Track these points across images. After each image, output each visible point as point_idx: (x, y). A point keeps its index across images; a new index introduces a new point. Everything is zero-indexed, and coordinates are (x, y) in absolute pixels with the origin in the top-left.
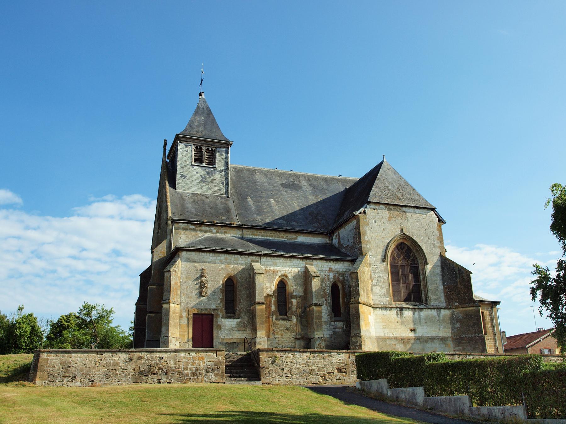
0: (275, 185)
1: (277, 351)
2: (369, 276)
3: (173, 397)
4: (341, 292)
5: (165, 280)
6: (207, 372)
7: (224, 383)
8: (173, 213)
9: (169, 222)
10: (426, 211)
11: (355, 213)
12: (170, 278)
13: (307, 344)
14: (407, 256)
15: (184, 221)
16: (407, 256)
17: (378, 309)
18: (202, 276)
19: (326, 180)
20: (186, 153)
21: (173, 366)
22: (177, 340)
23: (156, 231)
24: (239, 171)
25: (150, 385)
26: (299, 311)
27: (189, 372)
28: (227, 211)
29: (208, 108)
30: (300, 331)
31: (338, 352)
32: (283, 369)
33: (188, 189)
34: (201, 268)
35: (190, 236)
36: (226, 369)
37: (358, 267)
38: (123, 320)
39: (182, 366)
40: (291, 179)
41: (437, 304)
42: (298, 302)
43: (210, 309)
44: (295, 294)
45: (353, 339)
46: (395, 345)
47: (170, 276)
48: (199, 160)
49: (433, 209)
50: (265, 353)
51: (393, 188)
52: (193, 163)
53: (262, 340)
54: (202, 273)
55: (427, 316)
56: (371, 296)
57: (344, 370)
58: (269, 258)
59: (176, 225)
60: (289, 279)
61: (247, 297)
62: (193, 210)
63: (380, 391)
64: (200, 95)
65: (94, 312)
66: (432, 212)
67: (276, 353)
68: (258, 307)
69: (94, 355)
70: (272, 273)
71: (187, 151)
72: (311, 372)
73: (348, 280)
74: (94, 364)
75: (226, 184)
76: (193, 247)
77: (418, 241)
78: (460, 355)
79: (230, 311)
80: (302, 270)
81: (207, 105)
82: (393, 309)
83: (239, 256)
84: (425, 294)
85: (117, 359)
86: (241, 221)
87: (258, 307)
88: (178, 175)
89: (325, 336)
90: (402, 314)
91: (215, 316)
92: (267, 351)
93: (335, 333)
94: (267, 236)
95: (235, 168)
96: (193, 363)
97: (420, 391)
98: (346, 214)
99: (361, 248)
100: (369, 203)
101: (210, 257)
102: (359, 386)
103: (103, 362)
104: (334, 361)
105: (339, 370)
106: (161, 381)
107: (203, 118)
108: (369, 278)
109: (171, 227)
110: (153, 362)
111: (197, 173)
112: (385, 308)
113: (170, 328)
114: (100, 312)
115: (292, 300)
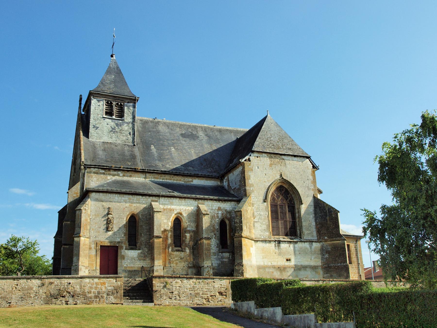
0: (176, 135)
1: (168, 277)
2: (252, 214)
3: (73, 315)
4: (228, 228)
5: (77, 217)
6: (108, 295)
7: (122, 304)
8: (86, 159)
9: (82, 167)
10: (302, 159)
11: (240, 160)
12: (81, 215)
13: (197, 271)
14: (285, 196)
15: (95, 167)
16: (285, 196)
17: (259, 242)
18: (108, 214)
19: (220, 131)
20: (98, 107)
21: (79, 290)
22: (86, 268)
23: (72, 174)
24: (144, 123)
25: (59, 306)
26: (192, 243)
27: (92, 295)
28: (133, 157)
29: (118, 68)
30: (192, 260)
31: (220, 279)
32: (173, 293)
33: (100, 138)
34: (108, 207)
35: (100, 179)
36: (124, 293)
37: (242, 207)
38: (46, 251)
39: (86, 291)
40: (190, 130)
41: (310, 238)
42: (191, 236)
43: (115, 242)
44: (188, 229)
45: (236, 268)
46: (273, 272)
47: (81, 213)
48: (109, 113)
49: (308, 158)
50: (157, 279)
51: (275, 139)
52: (105, 116)
53: (159, 268)
54: (109, 211)
55: (301, 248)
56: (253, 231)
57: (224, 294)
58: (166, 198)
59: (88, 170)
60: (183, 216)
61: (147, 232)
62: (103, 157)
63: (249, 311)
64: (112, 56)
65: (20, 244)
66: (308, 160)
67: (167, 279)
68: (156, 240)
69: (12, 281)
70: (168, 211)
71: (99, 106)
72: (197, 295)
73: (234, 218)
74: (11, 289)
75: (133, 134)
76: (101, 189)
77: (295, 185)
78: (324, 281)
79: (133, 243)
80: (195, 209)
81: (117, 65)
82: (272, 242)
83: (141, 197)
84: (300, 230)
85: (31, 285)
86: (145, 166)
87: (156, 240)
88: (91, 126)
89: (214, 265)
90: (280, 246)
91: (119, 248)
92: (160, 277)
93: (222, 262)
94: (167, 179)
95: (141, 120)
96: (96, 288)
97: (279, 310)
98: (235, 160)
99: (245, 191)
100: (253, 152)
101: (116, 197)
102: (233, 307)
103: (19, 287)
104: (216, 286)
105: (221, 293)
106: (69, 303)
107: (113, 76)
108: (252, 216)
109: (84, 171)
110: (62, 287)
111: (107, 124)
112: (265, 241)
113: (80, 258)
114: (25, 243)
115: (186, 234)
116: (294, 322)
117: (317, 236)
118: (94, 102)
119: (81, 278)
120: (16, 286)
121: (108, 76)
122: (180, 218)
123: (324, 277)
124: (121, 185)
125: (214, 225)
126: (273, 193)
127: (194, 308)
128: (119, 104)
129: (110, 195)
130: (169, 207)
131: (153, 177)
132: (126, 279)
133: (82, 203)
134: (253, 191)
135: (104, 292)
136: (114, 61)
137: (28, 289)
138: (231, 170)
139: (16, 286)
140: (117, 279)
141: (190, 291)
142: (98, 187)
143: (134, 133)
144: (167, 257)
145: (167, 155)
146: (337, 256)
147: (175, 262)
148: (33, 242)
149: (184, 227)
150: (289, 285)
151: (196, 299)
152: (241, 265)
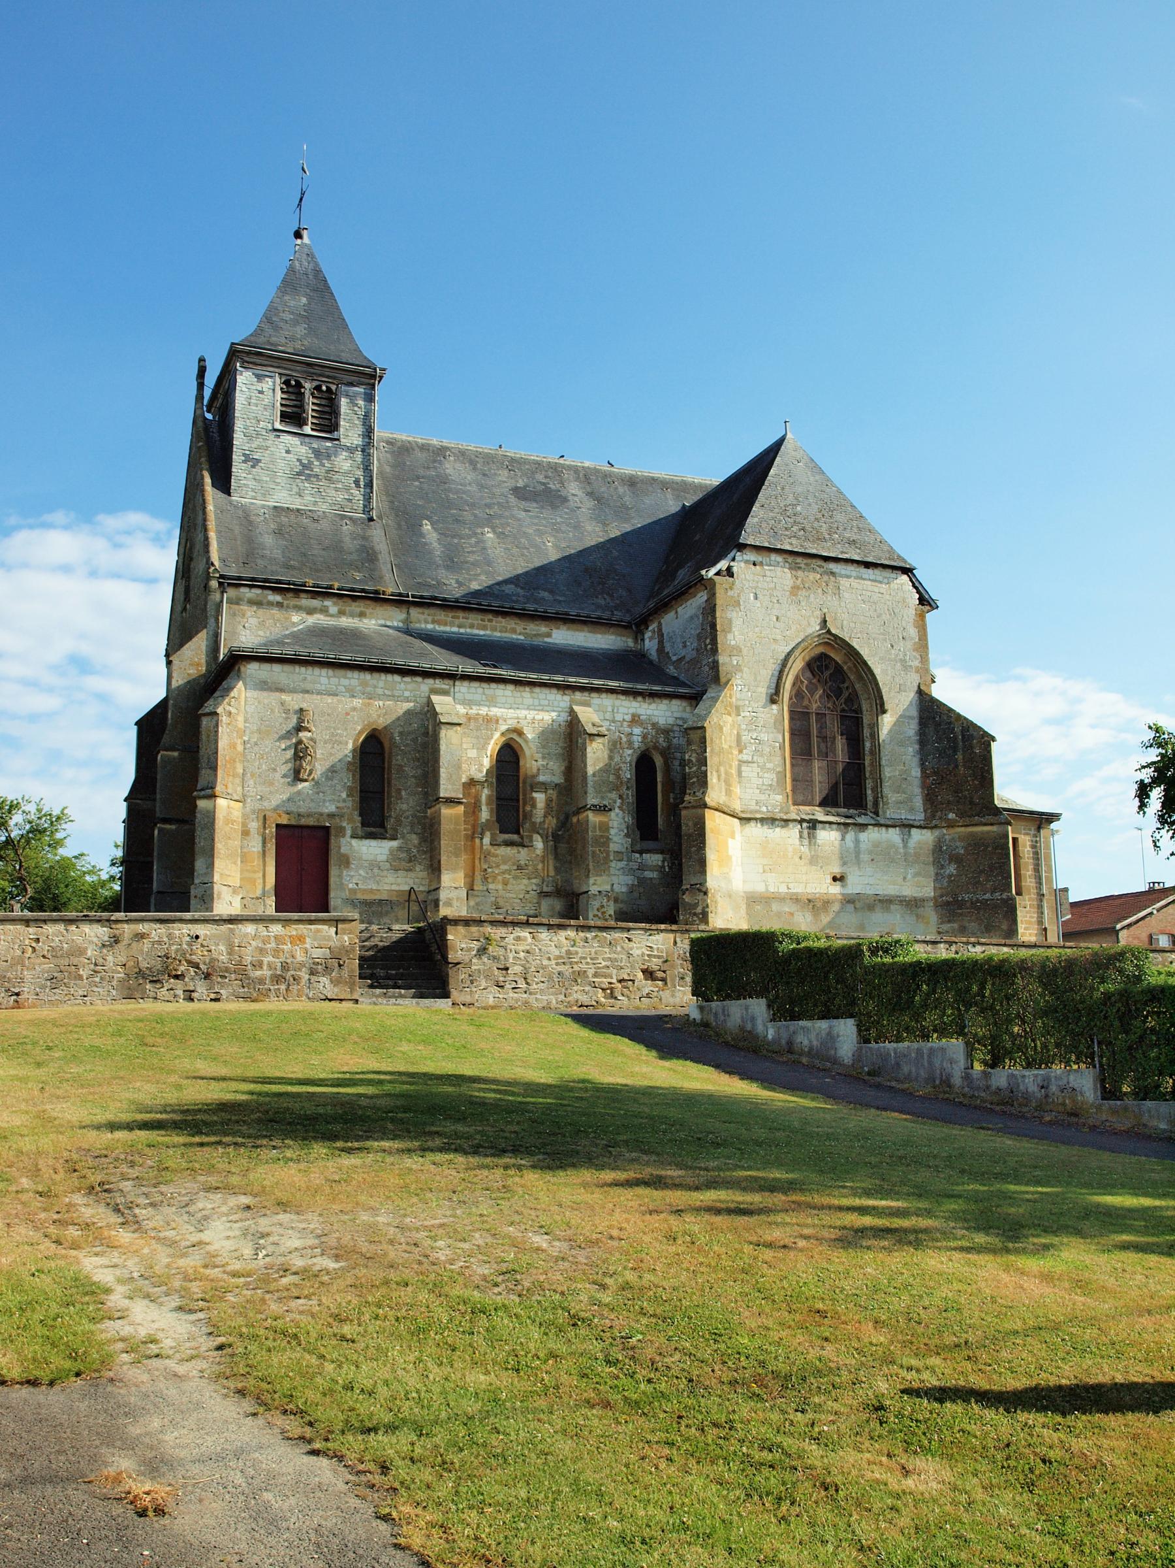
0: (497, 491)
2: (734, 738)
3: (225, 1034)
4: (659, 779)
5: (204, 737)
7: (357, 1001)
8: (223, 560)
9: (214, 584)
10: (888, 573)
11: (703, 572)
12: (217, 732)
13: (569, 906)
14: (834, 685)
15: (254, 583)
16: (834, 685)
17: (753, 824)
18: (299, 728)
19: (632, 482)
20: (257, 397)
21: (224, 958)
23: (179, 608)
24: (401, 451)
25: (165, 1004)
26: (551, 822)
27: (266, 972)
28: (369, 556)
29: (318, 272)
30: (552, 873)
31: (646, 930)
32: (507, 969)
33: (264, 495)
34: (297, 707)
35: (269, 622)
36: (361, 967)
38: (95, 836)
39: (248, 959)
40: (540, 477)
41: (904, 815)
42: (549, 801)
43: (321, 814)
44: (541, 778)
46: (792, 914)
47: (217, 725)
48: (293, 416)
49: (907, 571)
51: (808, 510)
52: (278, 426)
53: (453, 894)
54: (301, 720)
55: (877, 845)
56: (737, 790)
57: (660, 974)
58: (476, 684)
59: (231, 592)
60: (526, 741)
62: (277, 554)
63: (749, 1027)
64: (298, 235)
65: (17, 818)
66: (905, 577)
67: (488, 929)
68: (446, 812)
69: (20, 927)
70: (483, 724)
71: (261, 392)
73: (679, 748)
74: (19, 953)
76: (276, 651)
77: (865, 653)
78: (951, 943)
80: (561, 719)
81: (317, 264)
82: (791, 825)
83: (397, 678)
85: (79, 940)
86: (404, 586)
87: (446, 812)
88: (237, 457)
90: (815, 837)
91: (333, 832)
92: (467, 922)
93: (642, 881)
94: (472, 626)
96: (276, 952)
97: (846, 1030)
98: (681, 573)
99: (715, 666)
100: (742, 547)
101: (323, 678)
102: (695, 1015)
103: (43, 947)
104: (636, 952)
105: (649, 974)
106: (194, 995)
107: (304, 300)
108: (734, 744)
109: (217, 596)
110: (174, 948)
111: (288, 452)
112: (770, 821)
114: (33, 817)
115: (535, 795)
116: (898, 1064)
117: (925, 811)
118: (244, 379)
119: (232, 920)
120: (34, 944)
121: (287, 298)
122: (515, 746)
123: (939, 933)
124: (334, 639)
125: (620, 769)
126: (797, 677)
127: (566, 1016)
128: (324, 388)
129: (303, 669)
130: (484, 711)
131: (430, 619)
132: (363, 926)
133: (217, 694)
134: (738, 668)
135: (302, 965)
136: (306, 250)
137: (70, 954)
138: (670, 601)
139: (34, 944)
140: (340, 926)
141: (557, 964)
142: (265, 645)
143: (371, 481)
144: (477, 862)
145: (473, 552)
146: (981, 872)
147: (500, 878)
148: (54, 813)
149: (529, 773)
150: (880, 953)
151: (575, 988)
152: (700, 890)
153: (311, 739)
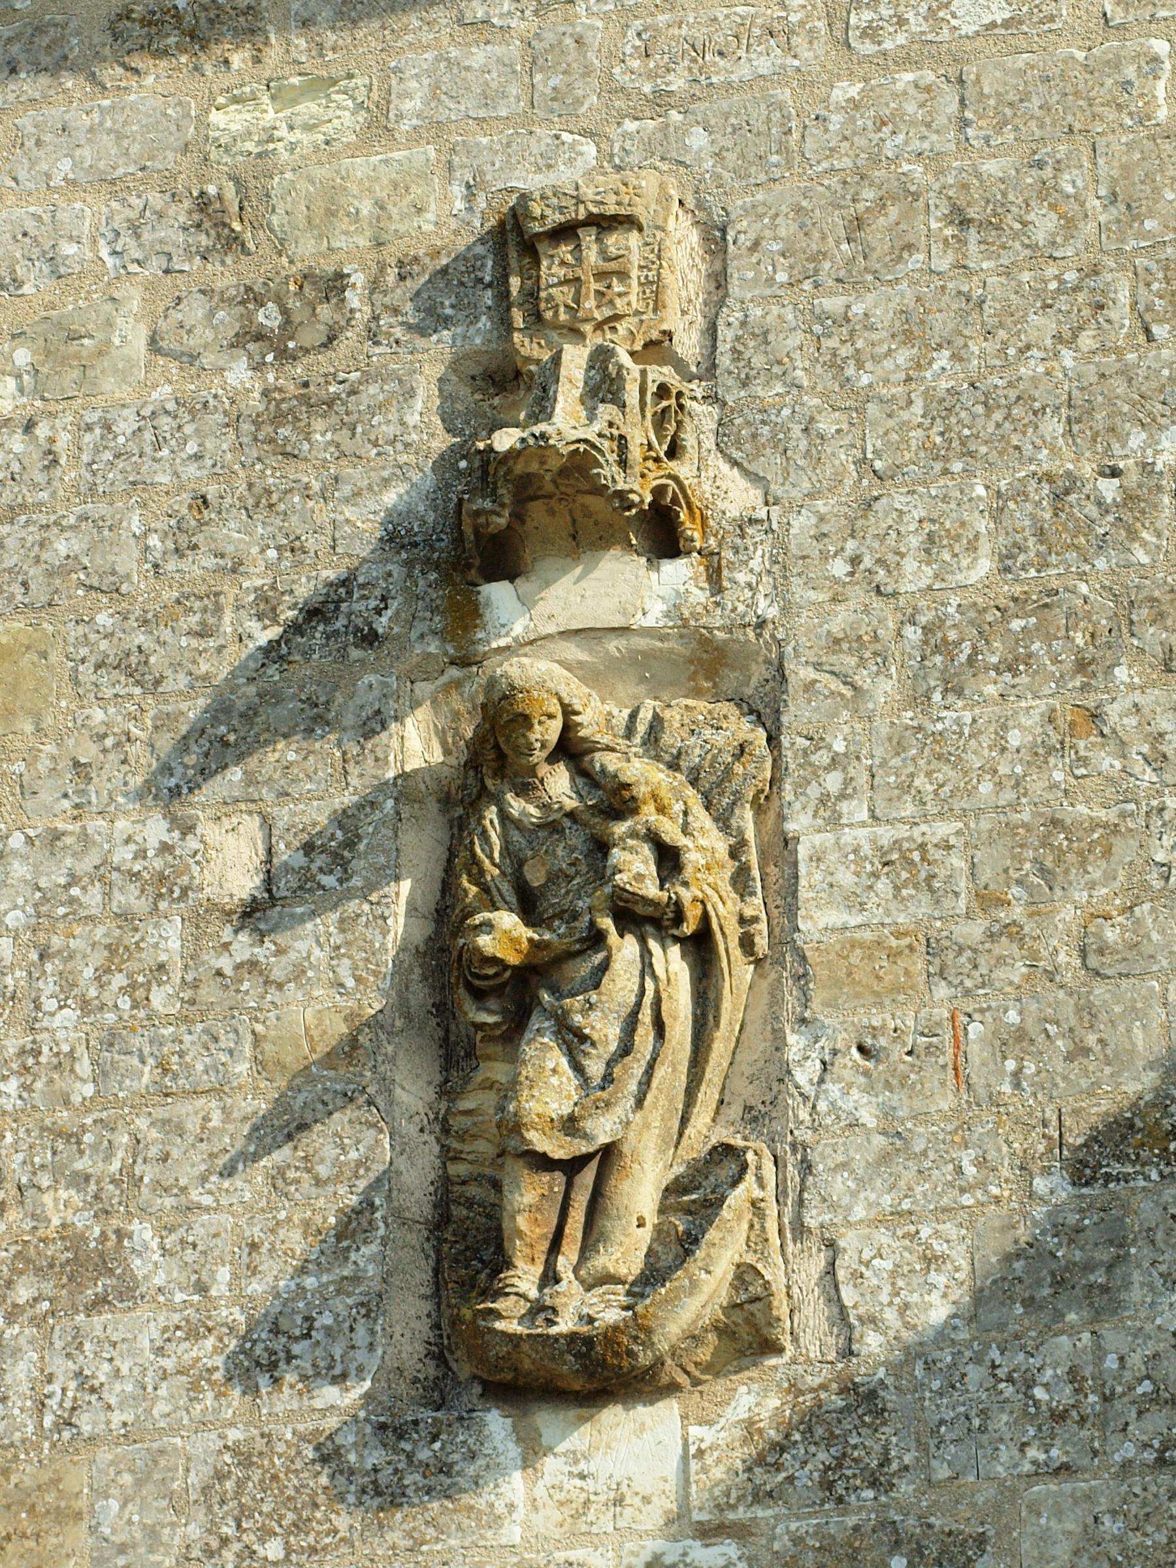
18: (489, 525)
34: (445, 221)
153: (703, 660)
